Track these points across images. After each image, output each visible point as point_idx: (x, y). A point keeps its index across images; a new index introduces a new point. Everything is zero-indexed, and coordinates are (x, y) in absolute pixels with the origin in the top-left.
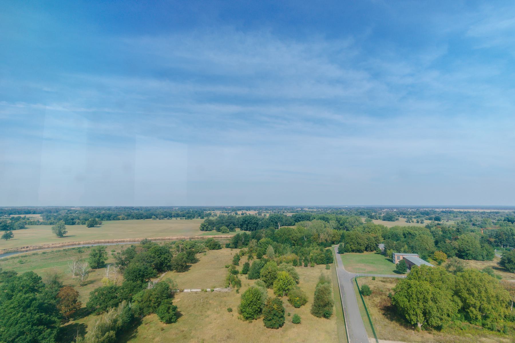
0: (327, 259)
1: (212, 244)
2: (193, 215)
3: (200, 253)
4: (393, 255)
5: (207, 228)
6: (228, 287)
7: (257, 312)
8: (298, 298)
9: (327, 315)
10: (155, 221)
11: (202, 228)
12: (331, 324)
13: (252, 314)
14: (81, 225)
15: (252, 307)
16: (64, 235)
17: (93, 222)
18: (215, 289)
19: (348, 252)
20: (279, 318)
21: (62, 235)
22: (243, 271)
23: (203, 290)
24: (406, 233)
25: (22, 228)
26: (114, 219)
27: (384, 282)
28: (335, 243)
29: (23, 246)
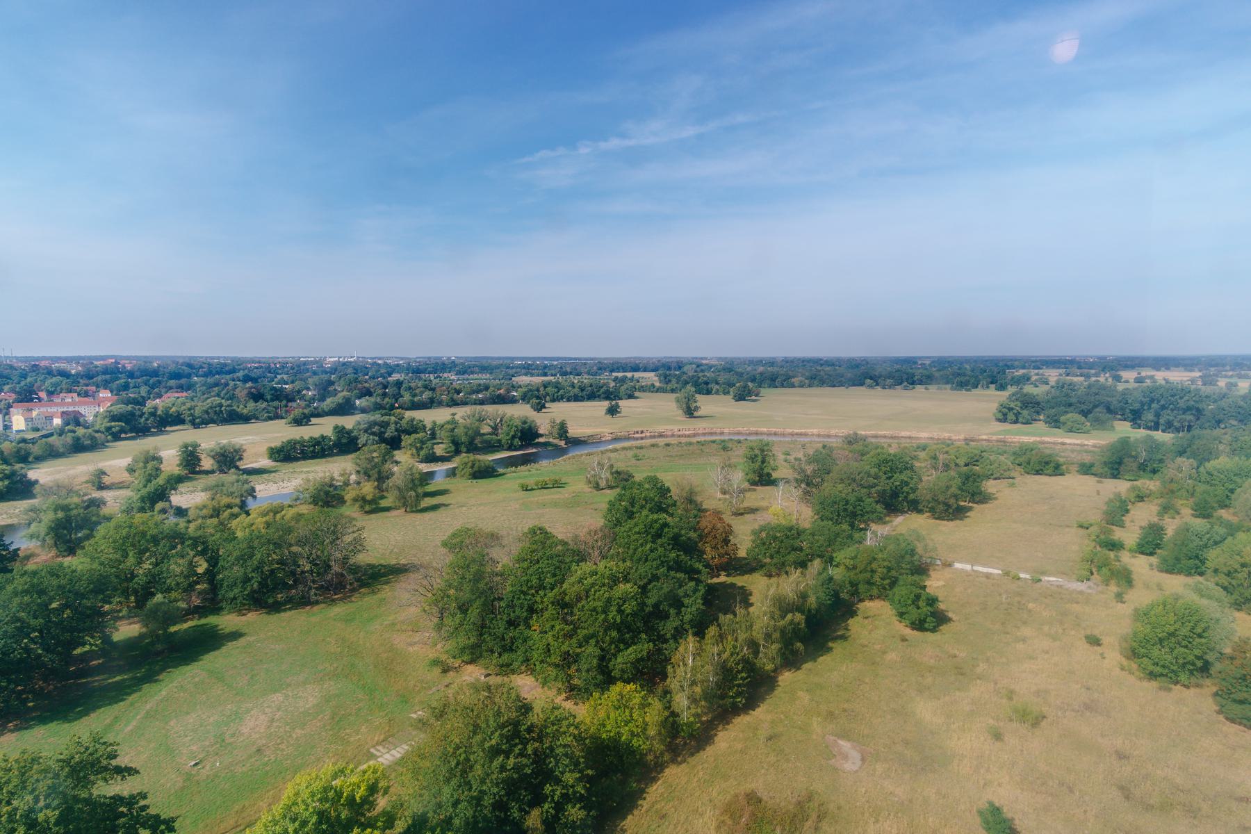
3: (995, 479)
5: (1017, 415)
10: (872, 392)
11: (1000, 416)
15: (1172, 649)
23: (1006, 574)
25: (631, 396)
26: (783, 386)
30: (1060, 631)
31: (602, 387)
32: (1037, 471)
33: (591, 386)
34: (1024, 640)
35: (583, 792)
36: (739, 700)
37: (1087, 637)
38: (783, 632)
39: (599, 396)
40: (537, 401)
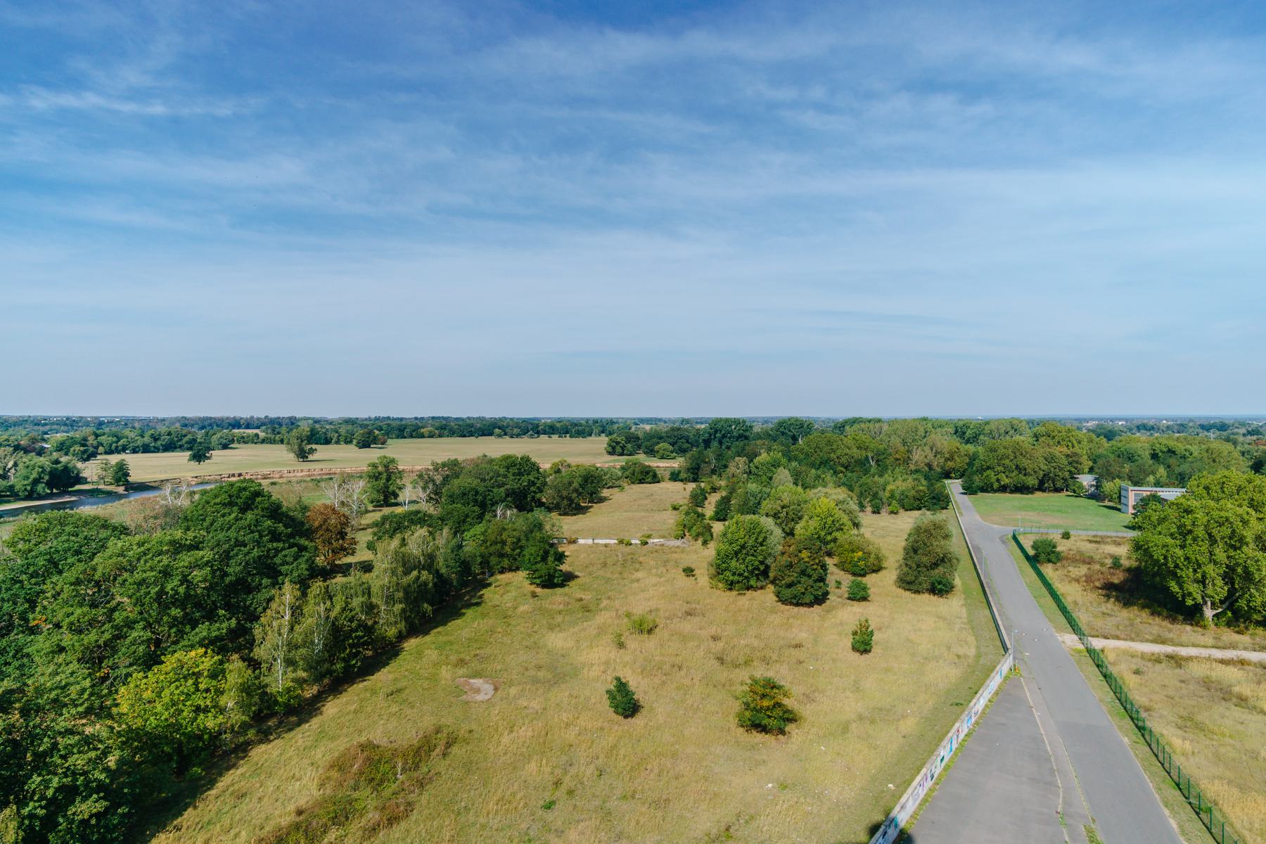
0: (934, 498)
1: (637, 470)
2: (587, 429)
3: (608, 488)
4: (1123, 493)
5: (623, 448)
6: (682, 538)
7: (757, 572)
8: (860, 554)
9: (940, 589)
10: (500, 440)
11: (610, 449)
12: (953, 605)
13: (746, 574)
14: (345, 446)
15: (744, 560)
16: (311, 457)
17: (369, 437)
18: (651, 541)
19: (989, 492)
20: (815, 581)
21: (307, 457)
22: (717, 513)
23: (621, 542)
24: (1161, 451)
25: (225, 447)
26: (412, 436)
27: (1096, 542)
28: (953, 475)
29: (231, 472)
30: (665, 571)
31: (185, 436)
32: (640, 480)
33: (169, 434)
34: (638, 581)
35: (102, 777)
36: (354, 662)
37: (684, 571)
38: (406, 592)
39: (181, 447)
40: (82, 448)
